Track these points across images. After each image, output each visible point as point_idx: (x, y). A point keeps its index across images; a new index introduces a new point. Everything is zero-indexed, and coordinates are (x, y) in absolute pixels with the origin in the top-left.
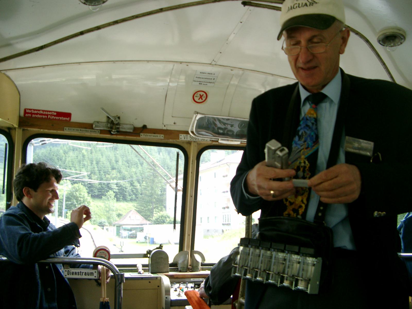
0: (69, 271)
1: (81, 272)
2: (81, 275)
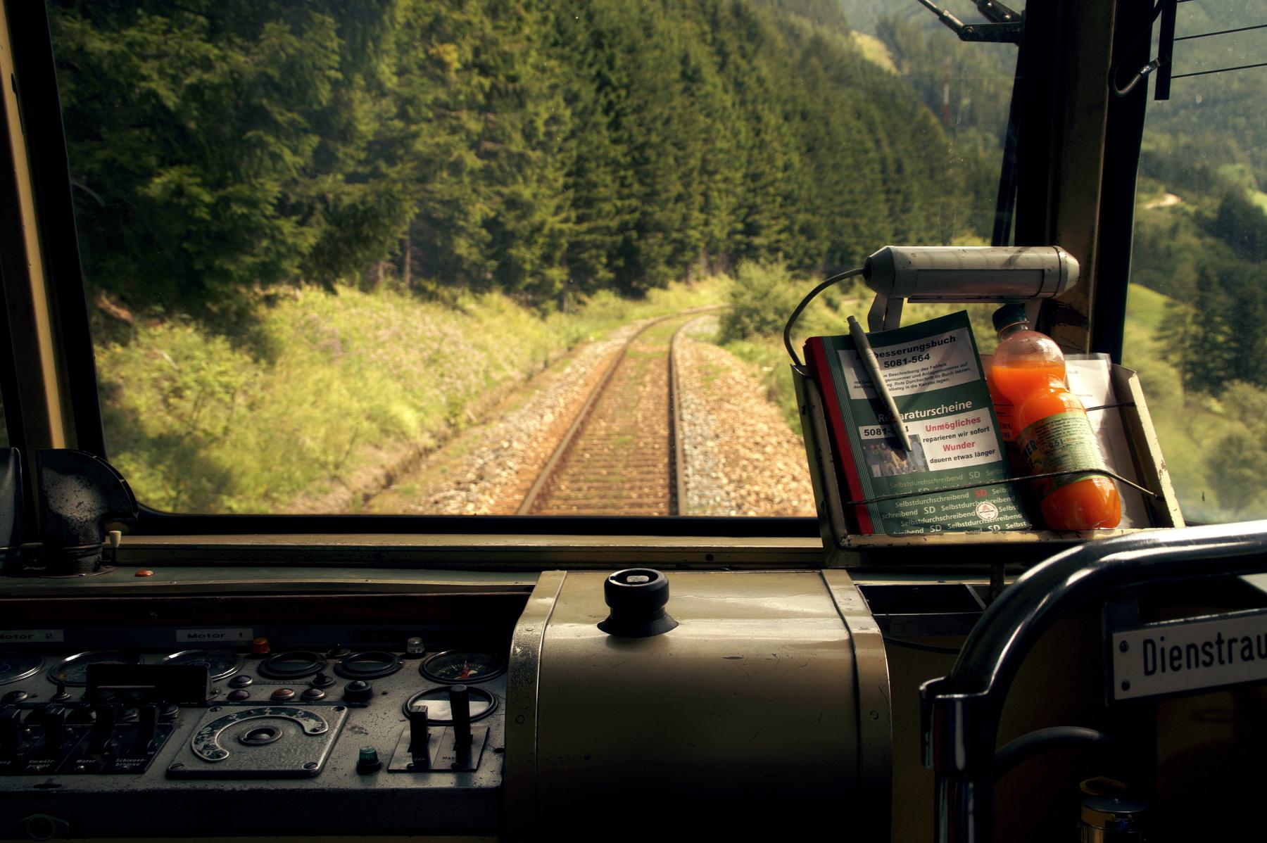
0: (1149, 646)
1: (1220, 642)
2: (1222, 662)
